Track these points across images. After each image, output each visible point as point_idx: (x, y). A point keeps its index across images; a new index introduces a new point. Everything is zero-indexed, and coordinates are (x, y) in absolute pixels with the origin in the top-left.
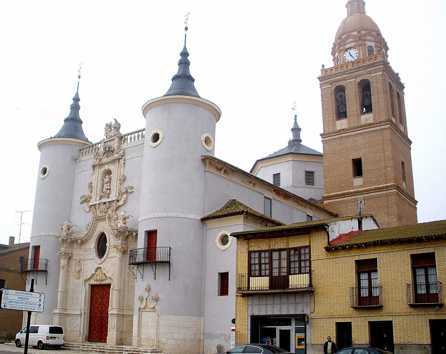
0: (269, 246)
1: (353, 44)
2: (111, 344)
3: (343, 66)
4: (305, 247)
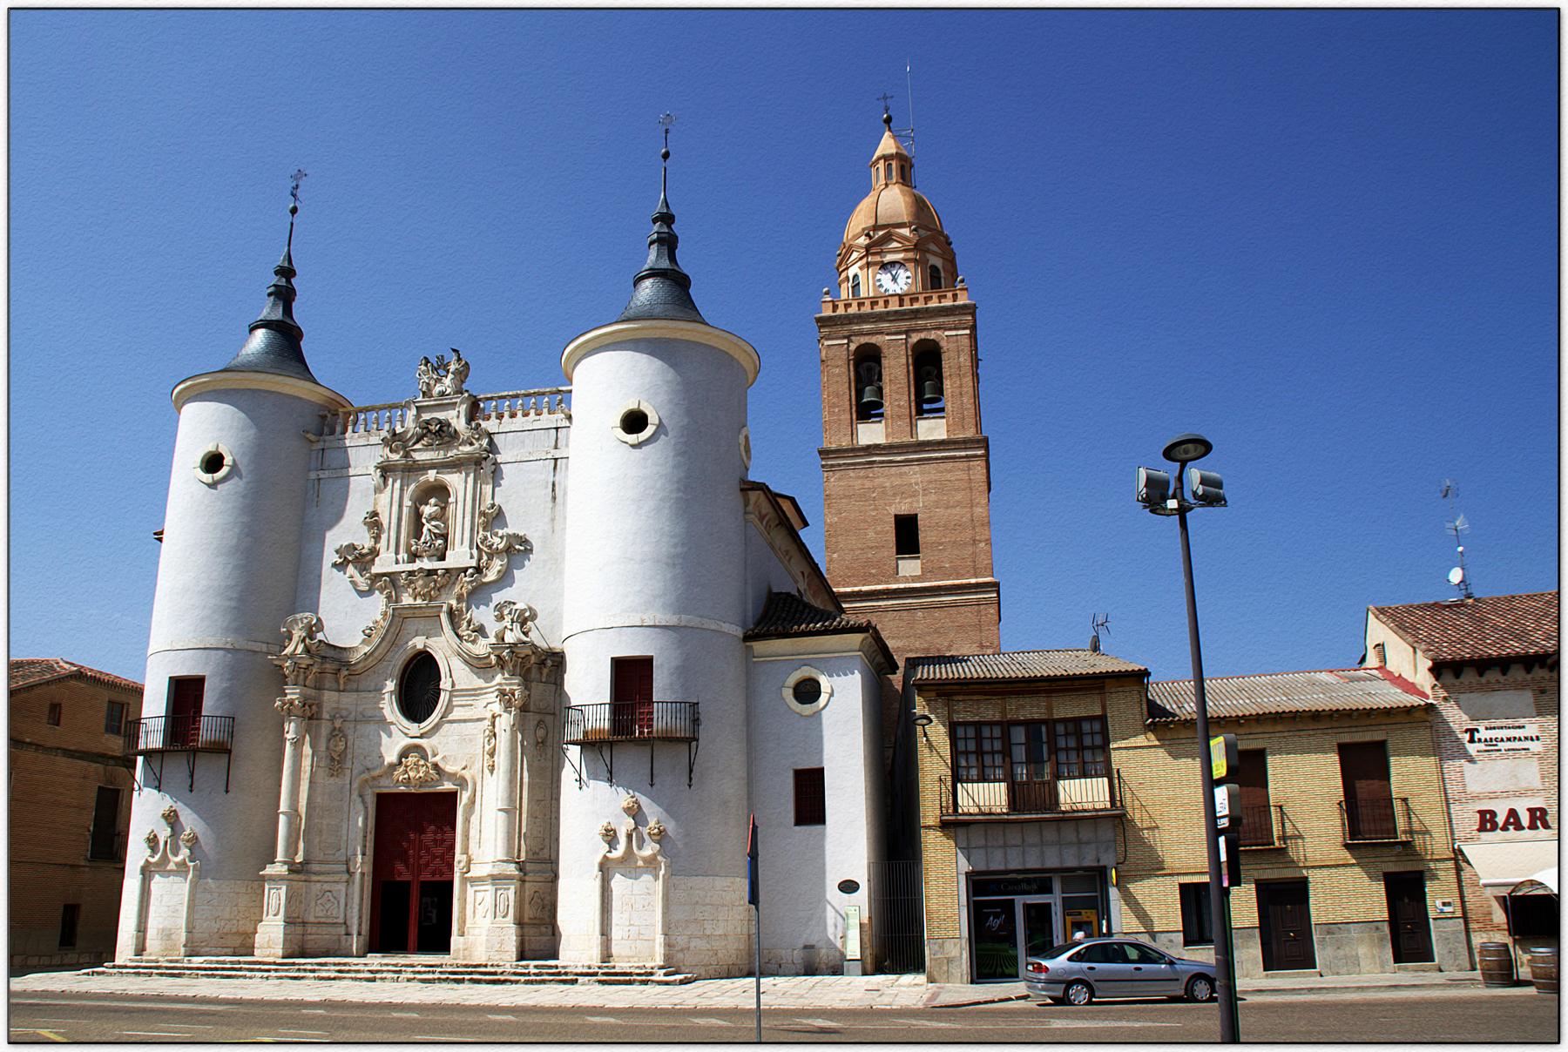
0: (1003, 712)
1: (901, 256)
3: (862, 301)
4: (1091, 719)
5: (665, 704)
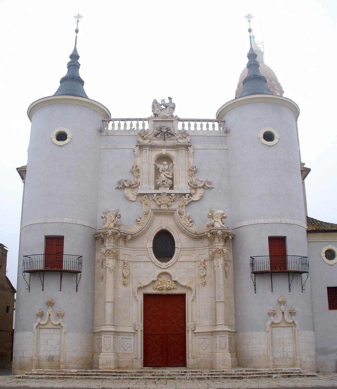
2: (224, 367)
5: (306, 258)
